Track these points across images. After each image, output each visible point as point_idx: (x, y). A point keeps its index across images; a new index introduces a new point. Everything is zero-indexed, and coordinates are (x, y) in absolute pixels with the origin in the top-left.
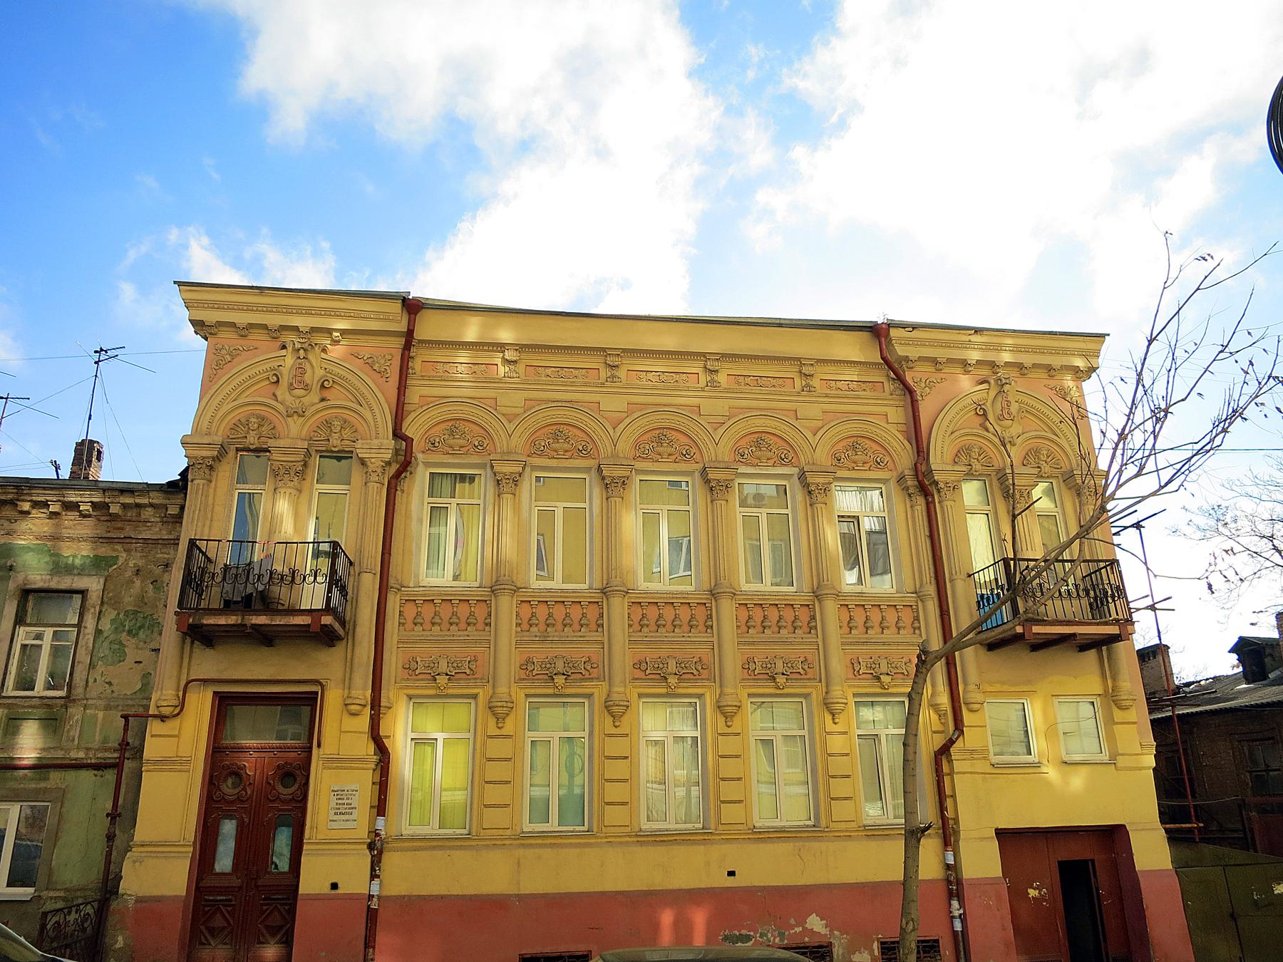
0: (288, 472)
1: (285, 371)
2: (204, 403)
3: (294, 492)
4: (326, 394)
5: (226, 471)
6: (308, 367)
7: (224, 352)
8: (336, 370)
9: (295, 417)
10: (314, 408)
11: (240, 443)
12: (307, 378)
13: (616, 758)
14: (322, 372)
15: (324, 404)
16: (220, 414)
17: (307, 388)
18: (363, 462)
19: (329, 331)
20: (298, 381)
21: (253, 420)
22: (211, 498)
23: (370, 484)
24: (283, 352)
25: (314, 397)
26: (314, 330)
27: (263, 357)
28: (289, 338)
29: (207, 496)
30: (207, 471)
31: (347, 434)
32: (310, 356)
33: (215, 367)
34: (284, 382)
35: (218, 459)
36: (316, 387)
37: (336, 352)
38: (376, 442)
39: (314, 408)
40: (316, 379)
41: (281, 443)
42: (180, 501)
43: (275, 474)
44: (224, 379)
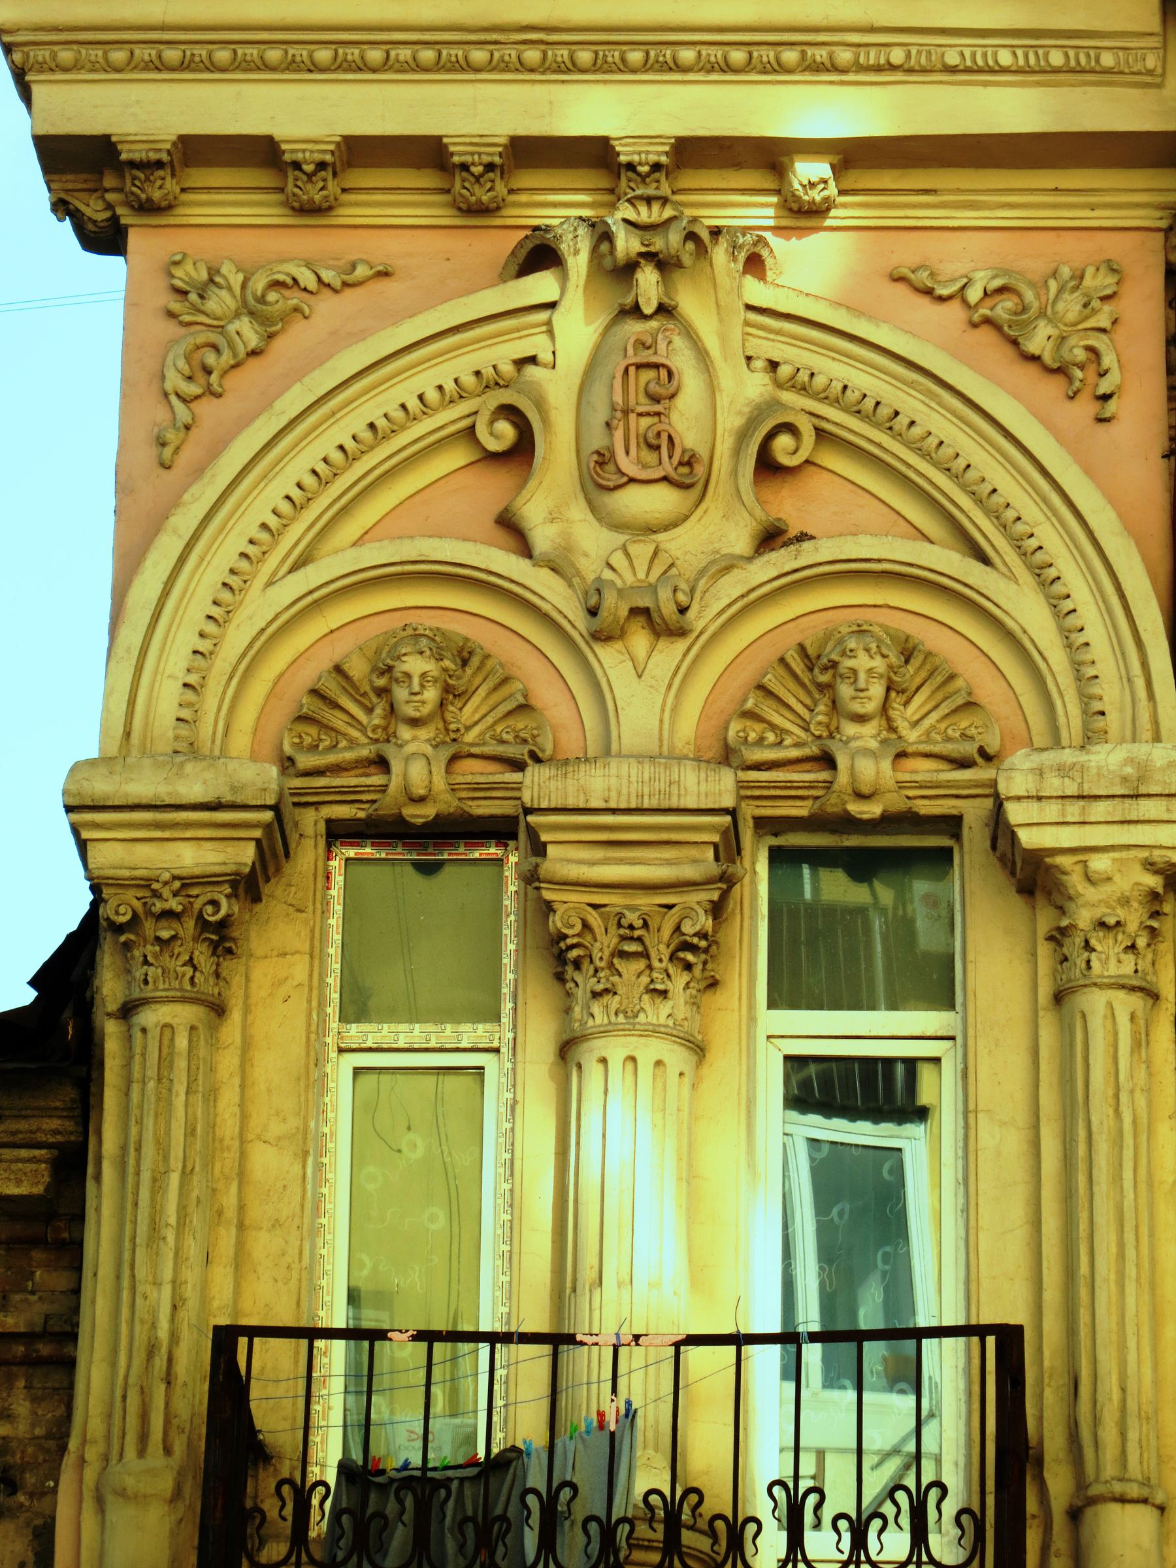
0: (632, 942)
1: (558, 388)
2: (132, 636)
3: (677, 1057)
4: (789, 505)
5: (294, 957)
6: (682, 360)
7: (220, 302)
8: (831, 370)
9: (640, 640)
10: (730, 588)
11: (347, 795)
12: (686, 419)
13: (605, 1106)
14: (757, 385)
15: (780, 561)
16: (237, 638)
17: (687, 475)
18: (1033, 878)
19: (768, 157)
20: (639, 443)
21: (415, 665)
22: (228, 1098)
23: (1095, 1002)
24: (542, 286)
25: (721, 527)
26: (692, 153)
27: (419, 319)
28: (559, 206)
29: (212, 1094)
30: (203, 956)
31: (917, 720)
32: (689, 302)
33: (189, 379)
34: (558, 450)
35: (248, 887)
36: (730, 469)
37: (811, 269)
38: (1109, 759)
39: (730, 588)
40: (729, 422)
41: (598, 784)
42: (52, 1127)
43: (560, 958)
44: (198, 511)
